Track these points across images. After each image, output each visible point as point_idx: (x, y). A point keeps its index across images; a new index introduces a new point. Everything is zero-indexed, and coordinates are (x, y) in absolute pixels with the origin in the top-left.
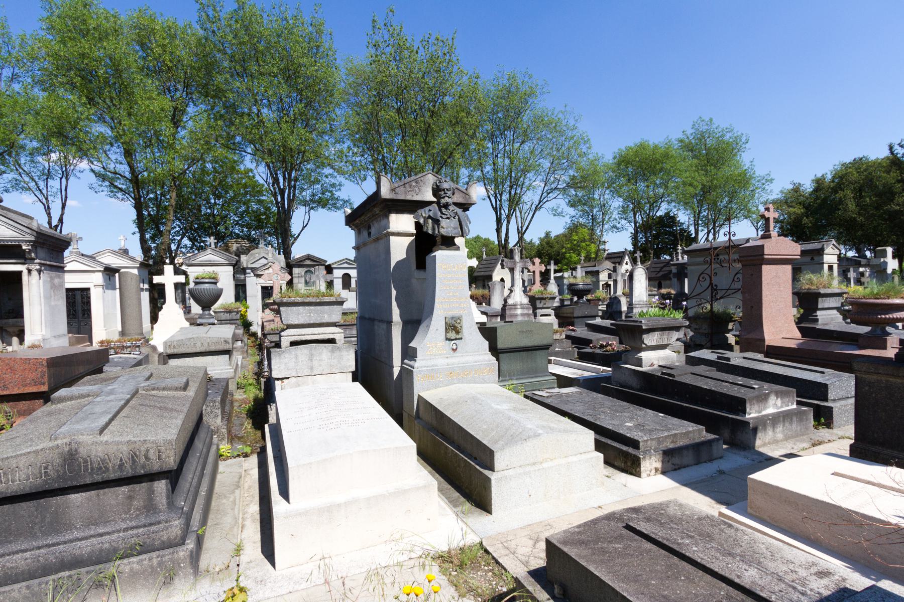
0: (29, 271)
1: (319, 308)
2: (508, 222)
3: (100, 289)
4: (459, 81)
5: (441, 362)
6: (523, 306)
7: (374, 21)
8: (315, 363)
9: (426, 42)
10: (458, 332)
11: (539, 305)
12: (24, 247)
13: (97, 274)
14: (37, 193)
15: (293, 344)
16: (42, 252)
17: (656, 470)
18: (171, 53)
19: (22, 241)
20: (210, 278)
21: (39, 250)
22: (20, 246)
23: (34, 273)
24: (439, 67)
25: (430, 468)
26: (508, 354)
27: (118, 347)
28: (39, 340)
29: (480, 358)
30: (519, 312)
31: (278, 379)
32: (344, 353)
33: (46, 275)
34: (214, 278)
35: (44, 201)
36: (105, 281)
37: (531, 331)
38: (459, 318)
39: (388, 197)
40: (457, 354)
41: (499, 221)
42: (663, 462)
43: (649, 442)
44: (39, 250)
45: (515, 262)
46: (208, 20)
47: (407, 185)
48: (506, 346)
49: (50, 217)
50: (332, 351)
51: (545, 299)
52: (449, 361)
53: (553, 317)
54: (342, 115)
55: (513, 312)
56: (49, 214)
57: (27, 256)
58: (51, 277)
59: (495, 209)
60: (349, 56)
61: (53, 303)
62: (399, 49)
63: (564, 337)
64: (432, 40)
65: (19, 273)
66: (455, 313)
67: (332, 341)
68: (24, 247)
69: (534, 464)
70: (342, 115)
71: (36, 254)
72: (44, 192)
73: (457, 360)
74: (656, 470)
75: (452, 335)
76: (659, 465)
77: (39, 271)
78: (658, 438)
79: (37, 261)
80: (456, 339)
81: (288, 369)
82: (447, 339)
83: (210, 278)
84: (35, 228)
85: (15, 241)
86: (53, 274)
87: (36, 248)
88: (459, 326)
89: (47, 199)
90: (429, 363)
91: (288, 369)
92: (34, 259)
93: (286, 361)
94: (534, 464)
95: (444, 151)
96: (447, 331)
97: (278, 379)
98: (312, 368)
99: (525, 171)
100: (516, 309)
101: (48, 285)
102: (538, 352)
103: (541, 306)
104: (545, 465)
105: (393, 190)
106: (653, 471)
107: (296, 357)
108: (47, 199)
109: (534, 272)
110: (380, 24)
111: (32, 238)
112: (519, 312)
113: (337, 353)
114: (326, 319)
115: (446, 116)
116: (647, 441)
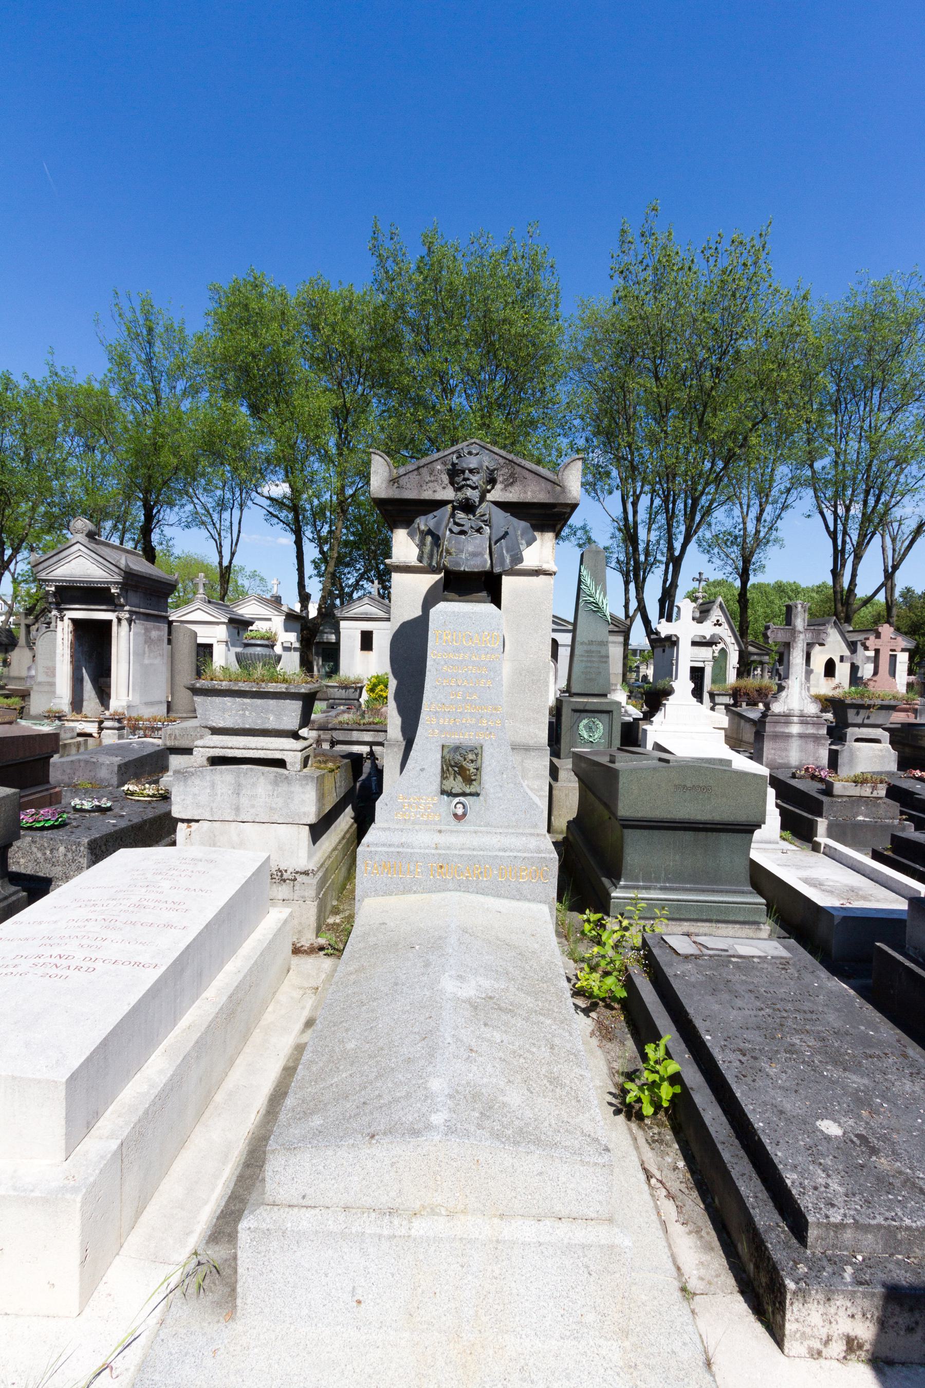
0: (119, 620)
1: (259, 702)
2: (858, 558)
3: (223, 646)
4: (770, 308)
5: (423, 840)
6: (804, 719)
7: (624, 231)
8: (244, 801)
9: (711, 252)
10: (469, 781)
11: (852, 717)
12: (113, 591)
13: (221, 626)
14: (210, 527)
15: (216, 761)
16: (134, 597)
17: (852, 1345)
18: (343, 333)
19: (111, 583)
20: (262, 638)
21: (130, 594)
22: (109, 589)
23: (125, 623)
24: (733, 293)
25: (858, 914)
26: (646, 832)
27: (146, 728)
28: (123, 707)
29: (533, 843)
30: (795, 729)
31: (183, 821)
32: (296, 788)
33: (138, 627)
34: (268, 639)
35: (217, 537)
36: (230, 635)
37: (706, 789)
38: (477, 751)
39: (383, 495)
40: (460, 826)
41: (838, 554)
42: (883, 1324)
43: (848, 1235)
44: (130, 594)
45: (794, 632)
46: (387, 279)
47: (424, 471)
48: (639, 815)
49: (221, 557)
50: (276, 782)
51: (869, 707)
52: (453, 839)
53: (886, 746)
54: (569, 393)
55: (780, 729)
56: (220, 553)
57: (116, 601)
58: (146, 630)
59: (833, 535)
60: (581, 302)
61: (146, 661)
62: (661, 270)
63: (883, 793)
64: (725, 245)
65: (110, 622)
66: (466, 738)
67: (280, 763)
68: (113, 591)
69: (392, 1212)
70: (569, 393)
71: (126, 599)
72: (218, 526)
73: (462, 839)
74: (852, 1345)
75: (457, 785)
76: (865, 1331)
77: (130, 621)
78: (891, 1232)
79: (127, 608)
80: (464, 794)
81: (198, 805)
82: (443, 792)
83: (262, 638)
84: (122, 566)
85: (104, 582)
86: (150, 624)
87: (127, 591)
88: (471, 767)
89: (219, 534)
90: (396, 838)
91: (198, 805)
92: (123, 606)
93: (196, 790)
94: (392, 1212)
95: (731, 433)
96: (444, 776)
97: (183, 821)
98: (237, 809)
99: (901, 462)
100: (788, 723)
101: (141, 639)
102: (724, 836)
103: (859, 720)
104: (420, 1227)
105: (394, 481)
106: (838, 1348)
107: (213, 785)
108: (219, 534)
109: (877, 651)
110: (633, 234)
111: (118, 579)
112: (795, 729)
113: (283, 788)
114: (272, 723)
115: (742, 373)
116: (840, 1226)
